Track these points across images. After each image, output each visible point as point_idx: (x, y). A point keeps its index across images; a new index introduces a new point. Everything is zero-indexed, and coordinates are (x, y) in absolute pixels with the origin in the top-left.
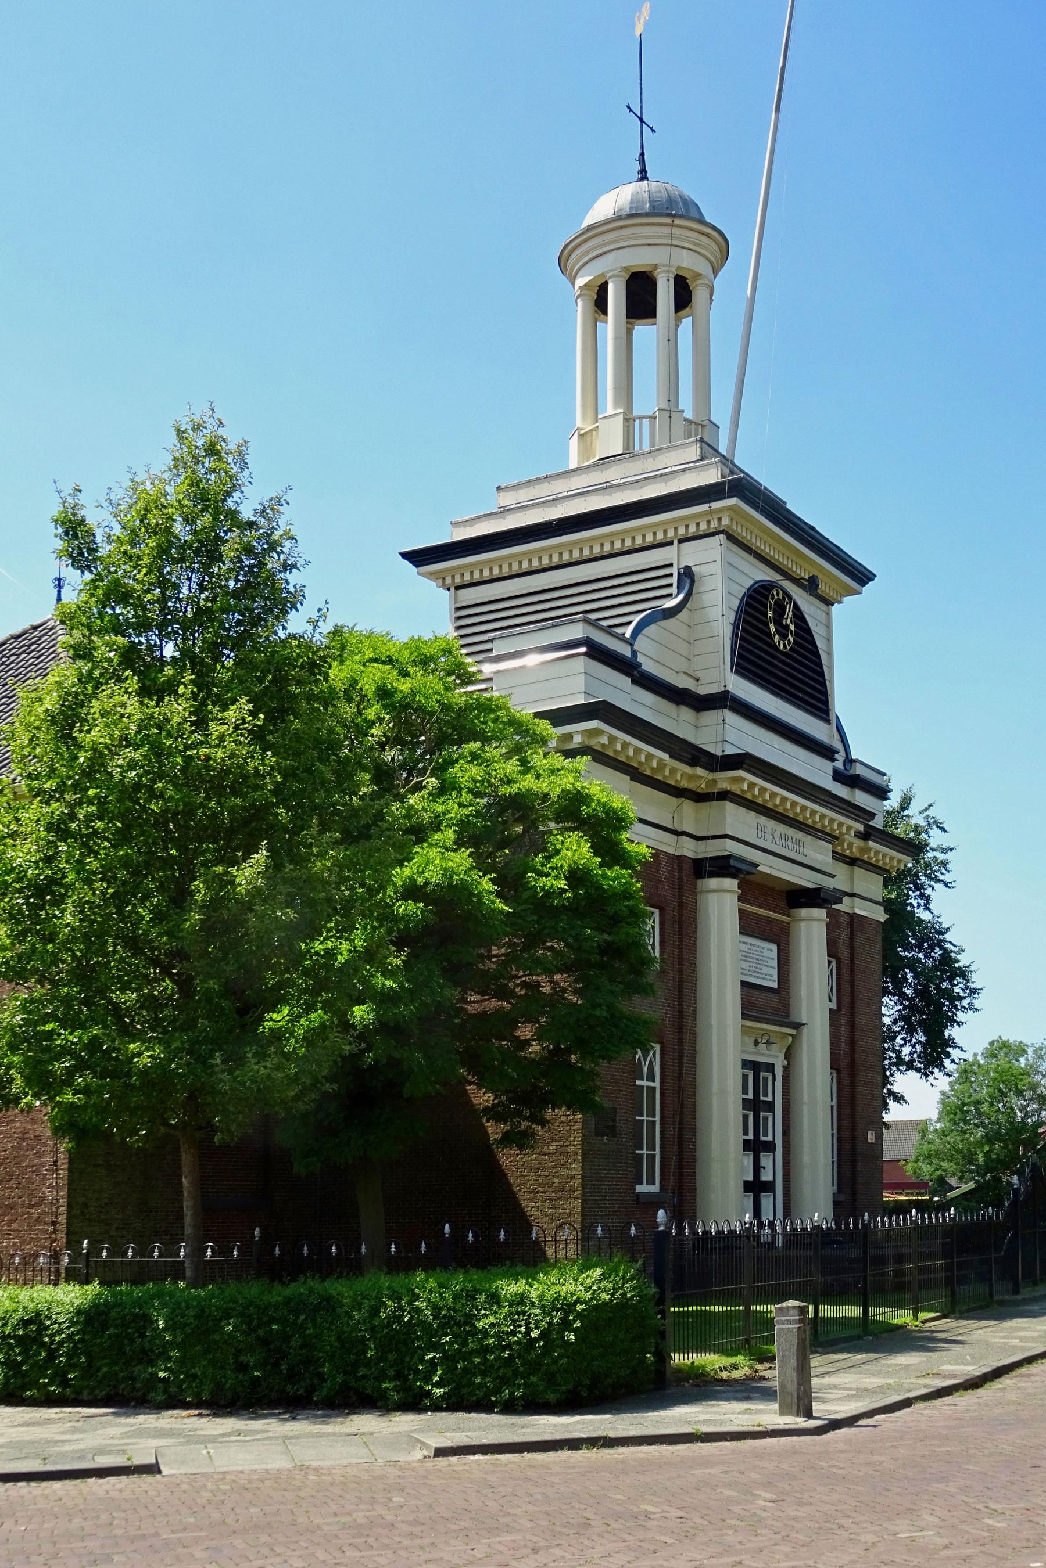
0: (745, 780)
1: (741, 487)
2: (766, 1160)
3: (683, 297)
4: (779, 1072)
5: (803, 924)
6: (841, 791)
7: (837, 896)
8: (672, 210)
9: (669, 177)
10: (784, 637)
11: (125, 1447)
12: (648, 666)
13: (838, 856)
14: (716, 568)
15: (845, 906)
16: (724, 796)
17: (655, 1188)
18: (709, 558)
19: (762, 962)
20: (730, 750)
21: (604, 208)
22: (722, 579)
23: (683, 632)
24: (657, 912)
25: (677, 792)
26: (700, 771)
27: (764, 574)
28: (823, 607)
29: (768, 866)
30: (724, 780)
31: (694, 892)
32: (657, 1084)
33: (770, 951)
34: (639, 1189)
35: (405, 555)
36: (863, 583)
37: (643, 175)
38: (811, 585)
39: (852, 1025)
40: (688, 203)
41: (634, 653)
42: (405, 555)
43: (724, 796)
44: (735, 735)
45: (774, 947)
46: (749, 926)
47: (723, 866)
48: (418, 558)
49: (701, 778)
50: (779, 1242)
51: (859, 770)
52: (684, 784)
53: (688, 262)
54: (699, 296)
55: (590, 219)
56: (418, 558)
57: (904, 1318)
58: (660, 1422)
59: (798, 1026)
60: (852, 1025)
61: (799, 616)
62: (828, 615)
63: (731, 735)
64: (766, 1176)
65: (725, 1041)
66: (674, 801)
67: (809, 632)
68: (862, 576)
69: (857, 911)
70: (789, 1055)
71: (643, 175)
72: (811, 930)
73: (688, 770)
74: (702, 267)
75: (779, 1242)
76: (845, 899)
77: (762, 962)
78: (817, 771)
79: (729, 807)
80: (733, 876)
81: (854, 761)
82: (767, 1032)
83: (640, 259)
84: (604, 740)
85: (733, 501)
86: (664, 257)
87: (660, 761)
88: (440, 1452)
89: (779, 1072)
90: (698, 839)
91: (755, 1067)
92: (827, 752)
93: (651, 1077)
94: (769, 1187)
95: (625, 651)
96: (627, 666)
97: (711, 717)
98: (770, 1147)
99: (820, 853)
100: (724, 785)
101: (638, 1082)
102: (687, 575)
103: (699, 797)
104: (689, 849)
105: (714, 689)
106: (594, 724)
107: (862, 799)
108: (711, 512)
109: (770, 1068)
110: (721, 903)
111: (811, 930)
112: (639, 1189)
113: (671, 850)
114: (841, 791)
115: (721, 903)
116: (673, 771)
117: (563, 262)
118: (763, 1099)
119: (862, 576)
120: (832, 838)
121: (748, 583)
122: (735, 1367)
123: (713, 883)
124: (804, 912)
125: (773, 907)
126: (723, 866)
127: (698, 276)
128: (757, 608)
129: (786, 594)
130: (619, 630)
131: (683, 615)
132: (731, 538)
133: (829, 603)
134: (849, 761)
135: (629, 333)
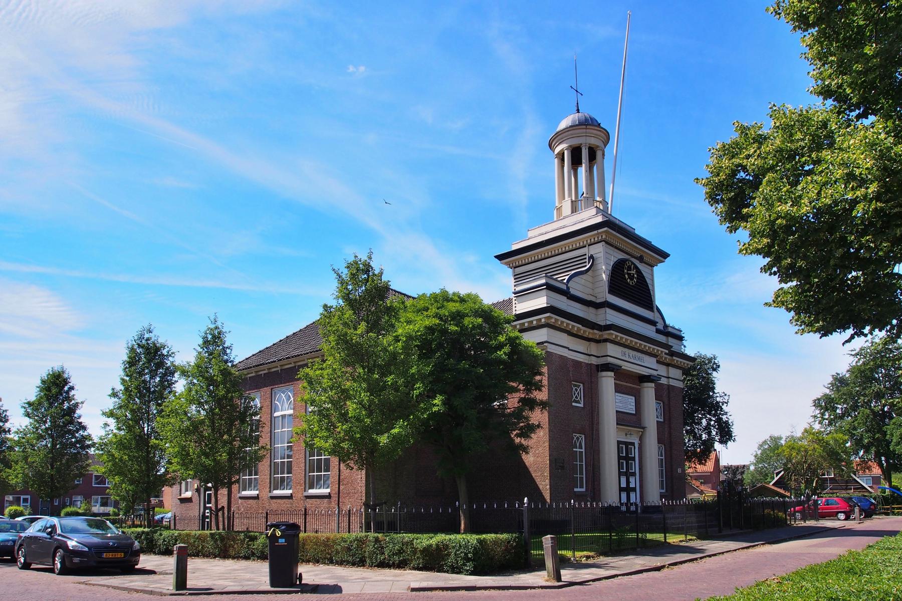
0: (614, 334)
1: (609, 224)
2: (632, 479)
3: (592, 157)
4: (637, 446)
6: (661, 338)
7: (659, 377)
8: (588, 123)
9: (588, 111)
10: (632, 279)
12: (572, 291)
13: (658, 362)
14: (602, 255)
15: (664, 381)
16: (606, 340)
17: (584, 490)
18: (598, 250)
19: (628, 404)
20: (608, 323)
21: (564, 124)
22: (604, 258)
23: (590, 279)
26: (595, 331)
27: (622, 256)
29: (626, 366)
30: (606, 335)
32: (583, 450)
33: (632, 399)
34: (576, 490)
35: (496, 257)
36: (665, 258)
37: (578, 111)
38: (641, 259)
39: (670, 427)
40: (592, 119)
41: (568, 288)
42: (496, 257)
43: (606, 340)
44: (611, 317)
46: (618, 389)
47: (607, 367)
48: (500, 257)
49: (596, 334)
50: (639, 511)
51: (670, 330)
52: (590, 336)
53: (593, 141)
54: (599, 154)
55: (558, 130)
56: (500, 257)
57: (674, 539)
58: (446, 580)
59: (644, 428)
60: (670, 427)
61: (639, 272)
62: (652, 270)
63: (609, 317)
64: (632, 485)
65: (611, 435)
66: (588, 343)
67: (644, 277)
68: (665, 255)
70: (641, 439)
71: (578, 111)
72: (649, 391)
73: (591, 331)
74: (600, 144)
75: (639, 511)
76: (663, 379)
77: (628, 404)
78: (648, 331)
79: (609, 345)
80: (612, 371)
82: (630, 430)
83: (575, 142)
84: (553, 320)
85: (606, 229)
86: (586, 140)
87: (578, 328)
88: (413, 590)
89: (637, 446)
91: (627, 444)
92: (653, 323)
94: (634, 489)
95: (564, 287)
96: (566, 293)
97: (602, 311)
98: (634, 474)
99: (651, 362)
100: (606, 337)
102: (591, 257)
103: (598, 341)
104: (594, 361)
105: (603, 300)
106: (548, 314)
107: (671, 341)
108: (598, 234)
109: (633, 444)
110: (608, 381)
111: (649, 391)
112: (576, 490)
114: (661, 338)
115: (608, 381)
116: (585, 331)
117: (550, 146)
118: (625, 456)
119: (665, 255)
120: (654, 356)
121: (616, 260)
122: (588, 557)
123: (604, 373)
124: (646, 384)
125: (631, 383)
126: (607, 367)
127: (598, 146)
128: (618, 270)
129: (633, 263)
131: (590, 273)
132: (607, 243)
133: (652, 266)
134: (666, 326)
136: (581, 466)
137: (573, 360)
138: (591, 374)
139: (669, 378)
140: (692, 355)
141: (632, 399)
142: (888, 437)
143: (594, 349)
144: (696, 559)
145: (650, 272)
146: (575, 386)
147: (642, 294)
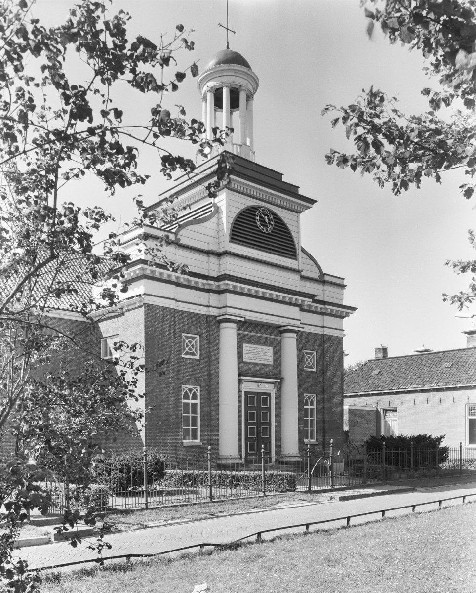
5: (286, 339)
11: (165, 523)
12: (183, 241)
24: (198, 337)
25: (209, 291)
28: (296, 214)
30: (223, 284)
31: (218, 330)
33: (269, 351)
44: (231, 266)
45: (271, 349)
49: (214, 285)
51: (327, 278)
53: (237, 80)
66: (206, 294)
67: (284, 224)
69: (325, 333)
72: (290, 343)
78: (291, 281)
79: (228, 295)
81: (325, 274)
90: (219, 308)
93: (312, 404)
99: (294, 312)
100: (223, 287)
101: (305, 407)
103: (219, 292)
104: (213, 312)
111: (290, 343)
113: (205, 313)
115: (229, 335)
130: (172, 231)
133: (299, 212)
134: (323, 275)
135: (215, 115)
136: (312, 421)
137: (184, 312)
138: (209, 326)
139: (323, 327)
140: (216, 276)
141: (269, 351)
142: (62, 281)
143: (214, 299)
144: (181, 523)
145: (296, 218)
146: (307, 354)
147: (281, 241)
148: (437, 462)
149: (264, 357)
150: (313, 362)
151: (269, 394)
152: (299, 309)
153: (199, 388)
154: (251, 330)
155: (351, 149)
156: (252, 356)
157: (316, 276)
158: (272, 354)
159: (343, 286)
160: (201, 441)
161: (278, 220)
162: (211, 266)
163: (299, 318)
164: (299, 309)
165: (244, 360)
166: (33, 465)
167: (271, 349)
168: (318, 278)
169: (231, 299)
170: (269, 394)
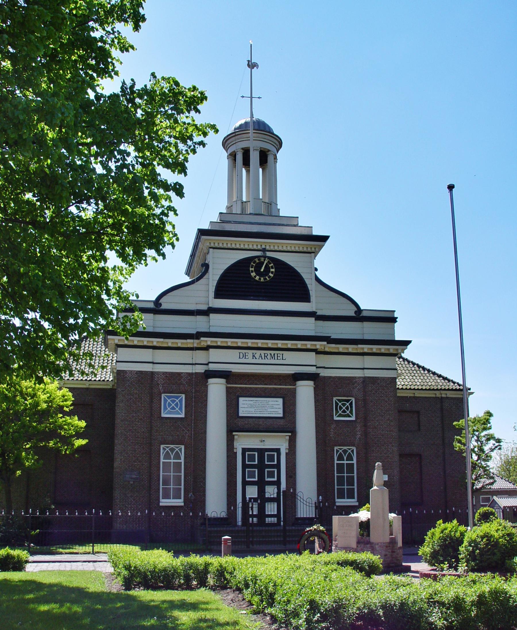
45: (280, 401)
49: (195, 343)
51: (364, 314)
99: (310, 358)
115: (216, 391)
134: (359, 310)
143: (200, 356)
147: (289, 285)
148: (237, 528)
149: (269, 410)
150: (351, 410)
151: (278, 451)
152: (314, 353)
153: (183, 447)
154: (240, 385)
155: (171, 213)
156: (253, 410)
157: (351, 312)
158: (281, 406)
159: (394, 320)
160: (185, 502)
161: (280, 264)
162: (199, 324)
163: (315, 364)
164: (314, 353)
165: (240, 415)
166: (265, 521)
167: (280, 401)
168: (354, 315)
169: (215, 355)
170: (278, 451)
